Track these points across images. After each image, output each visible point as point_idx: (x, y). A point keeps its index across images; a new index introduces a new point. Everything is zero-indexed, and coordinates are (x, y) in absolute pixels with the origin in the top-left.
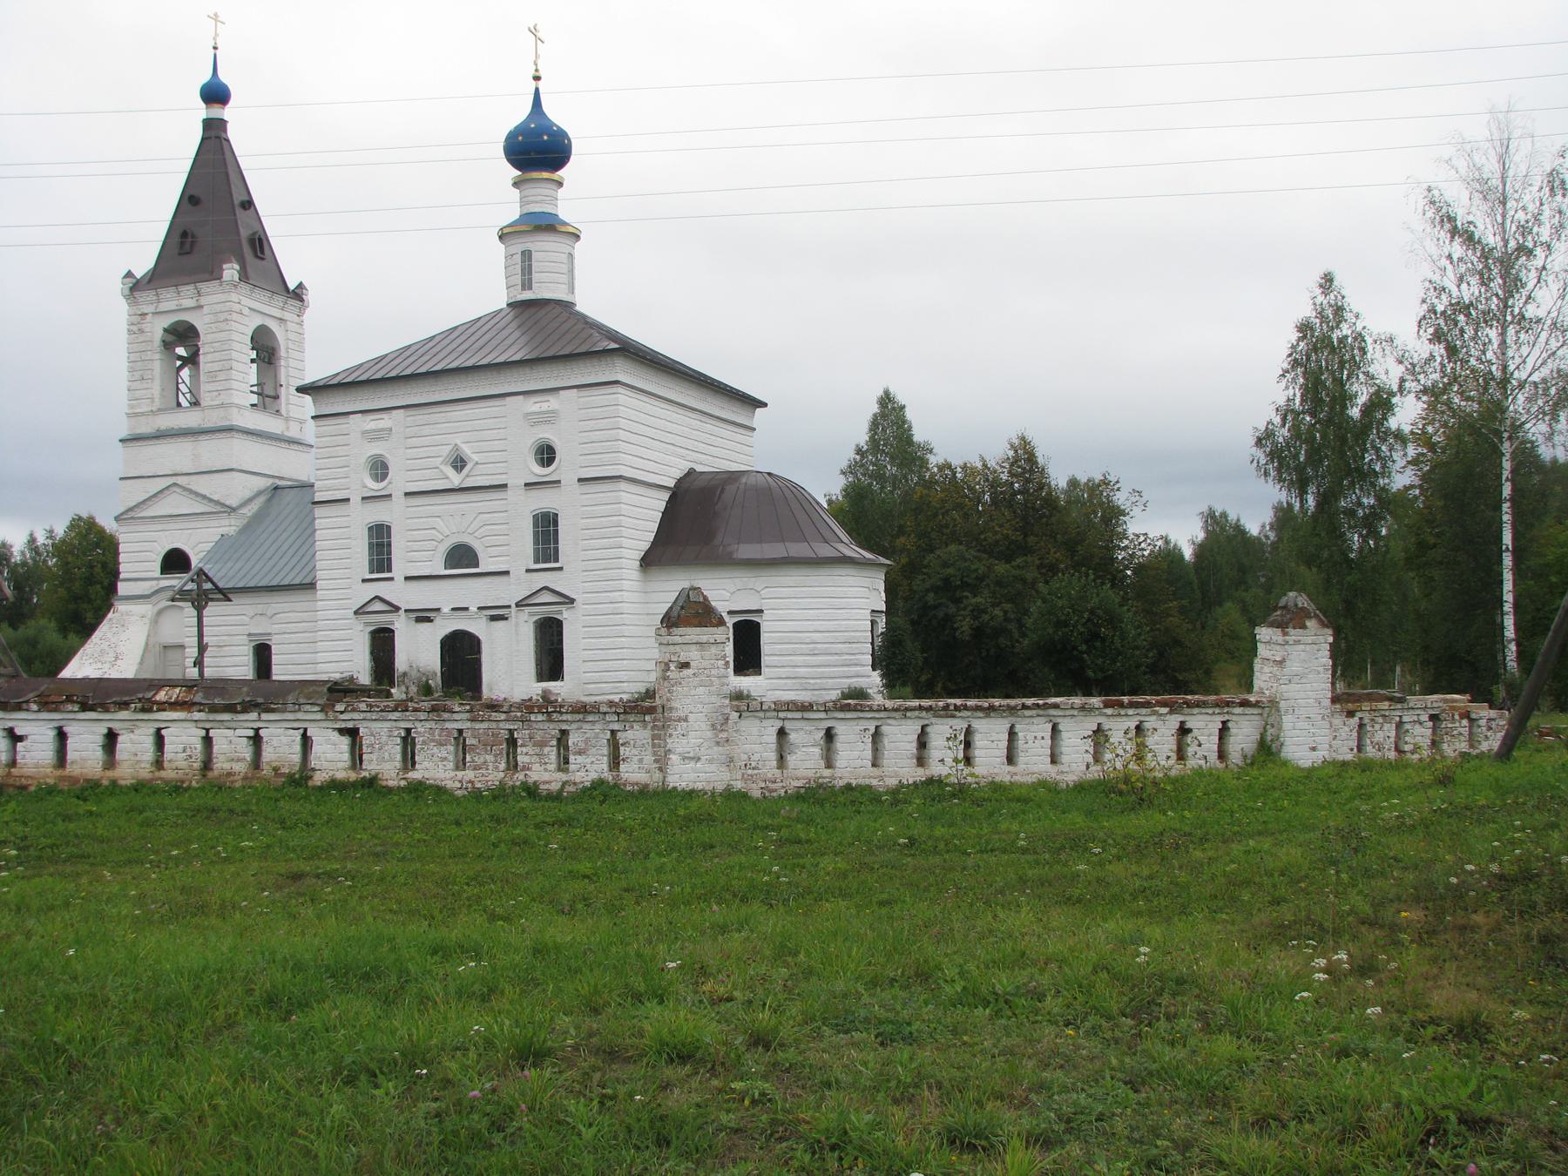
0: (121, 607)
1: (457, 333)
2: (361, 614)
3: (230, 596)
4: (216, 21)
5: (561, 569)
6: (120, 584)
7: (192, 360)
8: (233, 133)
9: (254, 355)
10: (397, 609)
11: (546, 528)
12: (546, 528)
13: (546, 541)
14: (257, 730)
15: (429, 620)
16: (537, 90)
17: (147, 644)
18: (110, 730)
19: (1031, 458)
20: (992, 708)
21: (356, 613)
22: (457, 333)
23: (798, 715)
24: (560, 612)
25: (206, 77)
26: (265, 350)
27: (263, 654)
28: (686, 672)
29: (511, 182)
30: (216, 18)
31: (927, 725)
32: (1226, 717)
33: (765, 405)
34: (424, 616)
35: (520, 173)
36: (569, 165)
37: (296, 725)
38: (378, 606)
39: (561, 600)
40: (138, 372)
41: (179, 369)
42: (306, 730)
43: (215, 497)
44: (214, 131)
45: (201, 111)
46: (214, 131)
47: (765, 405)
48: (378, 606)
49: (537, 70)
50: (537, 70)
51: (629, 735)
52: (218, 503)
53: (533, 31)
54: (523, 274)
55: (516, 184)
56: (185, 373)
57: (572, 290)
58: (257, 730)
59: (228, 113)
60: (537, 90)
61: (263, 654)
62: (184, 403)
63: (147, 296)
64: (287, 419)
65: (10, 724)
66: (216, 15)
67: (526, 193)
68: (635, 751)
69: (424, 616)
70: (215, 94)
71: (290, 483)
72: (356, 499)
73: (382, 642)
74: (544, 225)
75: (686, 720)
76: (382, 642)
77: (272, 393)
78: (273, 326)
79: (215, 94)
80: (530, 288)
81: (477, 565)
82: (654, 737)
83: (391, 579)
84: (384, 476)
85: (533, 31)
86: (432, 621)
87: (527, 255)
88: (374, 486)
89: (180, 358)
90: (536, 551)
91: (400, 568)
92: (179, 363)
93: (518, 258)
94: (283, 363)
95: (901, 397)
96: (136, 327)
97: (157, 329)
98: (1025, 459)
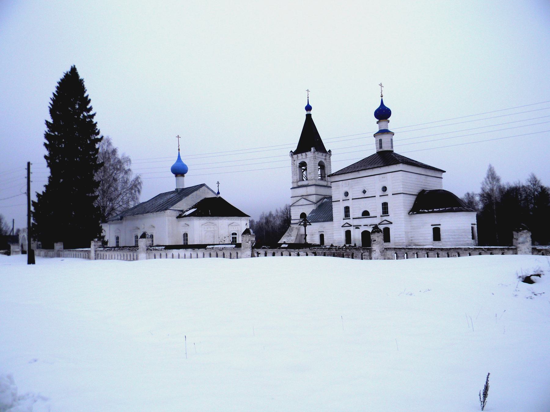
0: (292, 226)
1: (375, 155)
2: (344, 227)
3: (311, 223)
4: (308, 91)
5: (389, 216)
6: (291, 221)
7: (306, 170)
8: (313, 117)
9: (319, 167)
10: (351, 226)
11: (385, 206)
12: (385, 206)
13: (385, 209)
14: (298, 252)
15: (359, 228)
16: (382, 99)
17: (297, 234)
18: (274, 252)
19: (535, 178)
20: (73, 251)
21: (342, 227)
22: (375, 155)
23: (399, 250)
24: (389, 226)
25: (306, 104)
26: (322, 166)
27: (322, 237)
28: (375, 242)
29: (376, 123)
30: (308, 91)
31: (504, 252)
32: (503, 252)
33: (445, 172)
34: (357, 227)
35: (378, 120)
36: (390, 117)
37: (305, 251)
38: (347, 225)
39: (388, 223)
40: (294, 173)
41: (303, 171)
42: (307, 252)
43: (311, 201)
44: (309, 117)
45: (305, 113)
46: (309, 117)
47: (445, 172)
48: (347, 225)
49: (382, 94)
50: (382, 94)
51: (365, 254)
52: (312, 202)
53: (381, 85)
54: (380, 145)
55: (377, 123)
56: (305, 173)
57: (392, 147)
58: (298, 252)
59: (312, 112)
60: (382, 99)
61: (322, 237)
62: (305, 180)
63: (295, 156)
64: (327, 182)
65: (258, 251)
66: (308, 90)
67: (380, 125)
68: (366, 257)
69: (357, 227)
70: (308, 108)
71: (328, 197)
72: (341, 200)
73: (348, 233)
74: (384, 131)
75: (375, 251)
76: (348, 233)
77: (324, 176)
78: (323, 161)
79: (308, 108)
80: (382, 148)
81: (369, 215)
82: (369, 254)
83: (350, 219)
84: (347, 195)
85: (381, 85)
86: (359, 228)
87: (381, 140)
88: (345, 198)
89: (303, 169)
90: (383, 212)
91: (351, 216)
92: (303, 170)
93: (378, 141)
94: (326, 169)
95: (493, 165)
96: (293, 164)
97: (297, 163)
98: (534, 181)
